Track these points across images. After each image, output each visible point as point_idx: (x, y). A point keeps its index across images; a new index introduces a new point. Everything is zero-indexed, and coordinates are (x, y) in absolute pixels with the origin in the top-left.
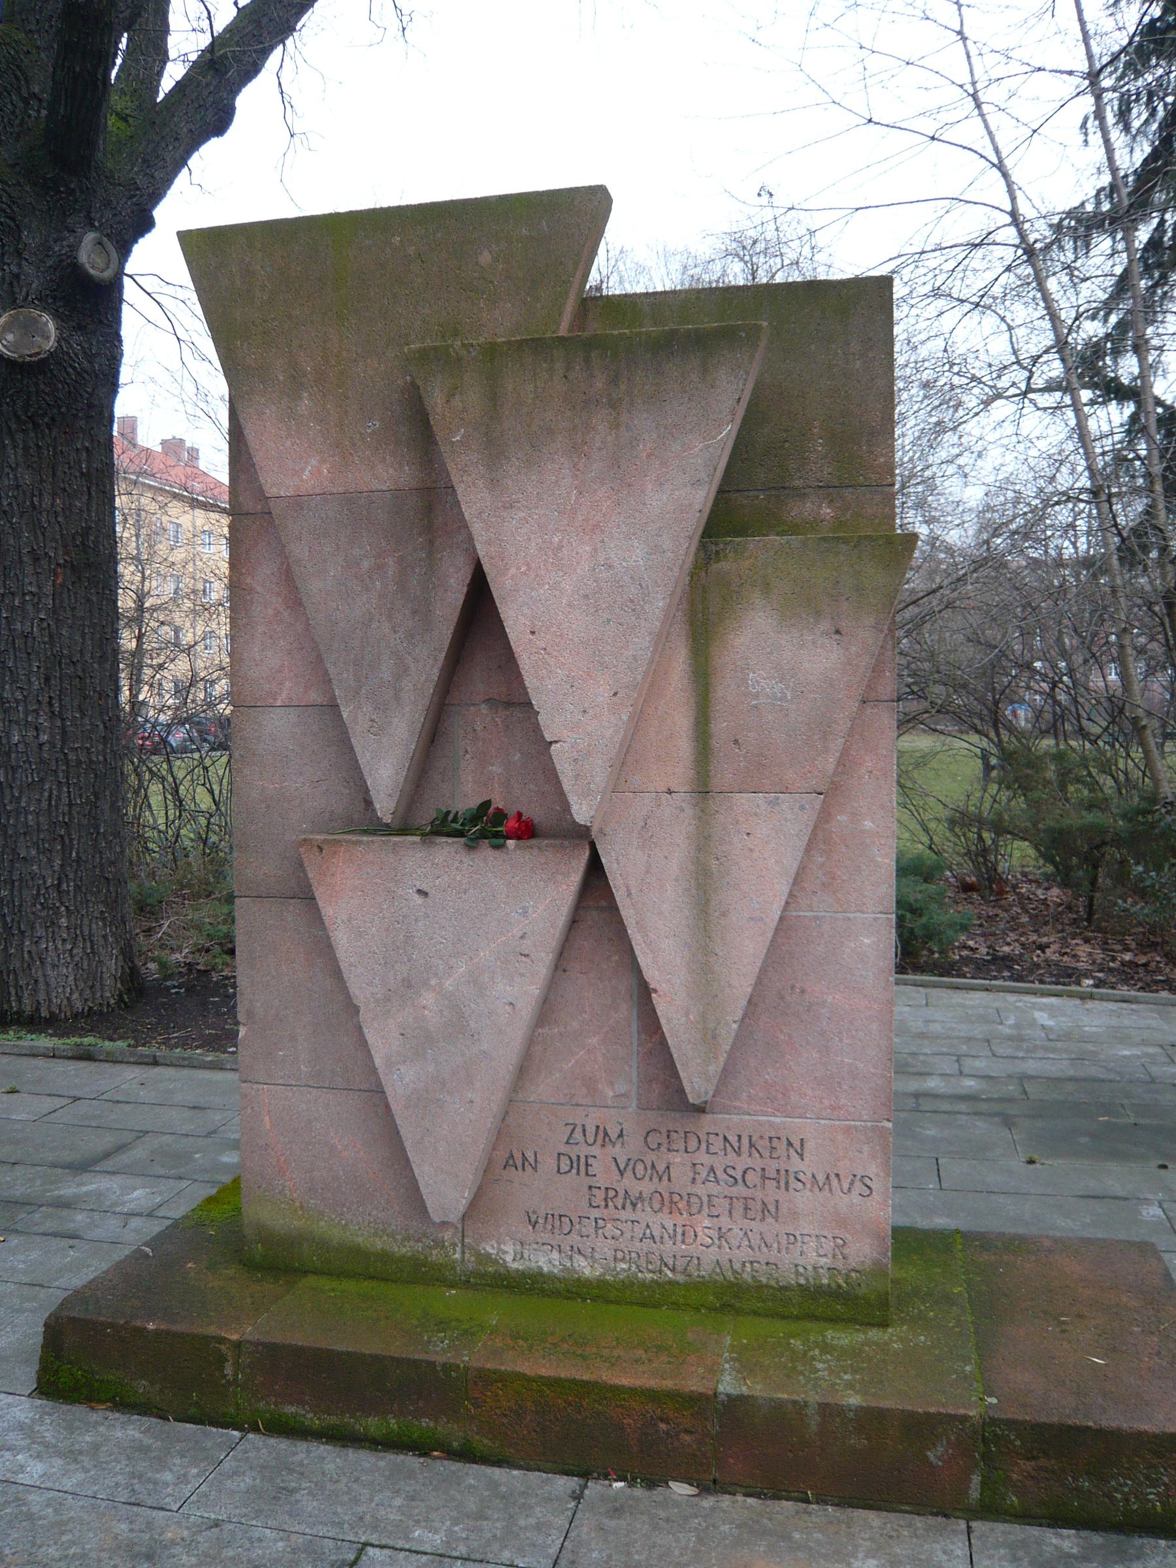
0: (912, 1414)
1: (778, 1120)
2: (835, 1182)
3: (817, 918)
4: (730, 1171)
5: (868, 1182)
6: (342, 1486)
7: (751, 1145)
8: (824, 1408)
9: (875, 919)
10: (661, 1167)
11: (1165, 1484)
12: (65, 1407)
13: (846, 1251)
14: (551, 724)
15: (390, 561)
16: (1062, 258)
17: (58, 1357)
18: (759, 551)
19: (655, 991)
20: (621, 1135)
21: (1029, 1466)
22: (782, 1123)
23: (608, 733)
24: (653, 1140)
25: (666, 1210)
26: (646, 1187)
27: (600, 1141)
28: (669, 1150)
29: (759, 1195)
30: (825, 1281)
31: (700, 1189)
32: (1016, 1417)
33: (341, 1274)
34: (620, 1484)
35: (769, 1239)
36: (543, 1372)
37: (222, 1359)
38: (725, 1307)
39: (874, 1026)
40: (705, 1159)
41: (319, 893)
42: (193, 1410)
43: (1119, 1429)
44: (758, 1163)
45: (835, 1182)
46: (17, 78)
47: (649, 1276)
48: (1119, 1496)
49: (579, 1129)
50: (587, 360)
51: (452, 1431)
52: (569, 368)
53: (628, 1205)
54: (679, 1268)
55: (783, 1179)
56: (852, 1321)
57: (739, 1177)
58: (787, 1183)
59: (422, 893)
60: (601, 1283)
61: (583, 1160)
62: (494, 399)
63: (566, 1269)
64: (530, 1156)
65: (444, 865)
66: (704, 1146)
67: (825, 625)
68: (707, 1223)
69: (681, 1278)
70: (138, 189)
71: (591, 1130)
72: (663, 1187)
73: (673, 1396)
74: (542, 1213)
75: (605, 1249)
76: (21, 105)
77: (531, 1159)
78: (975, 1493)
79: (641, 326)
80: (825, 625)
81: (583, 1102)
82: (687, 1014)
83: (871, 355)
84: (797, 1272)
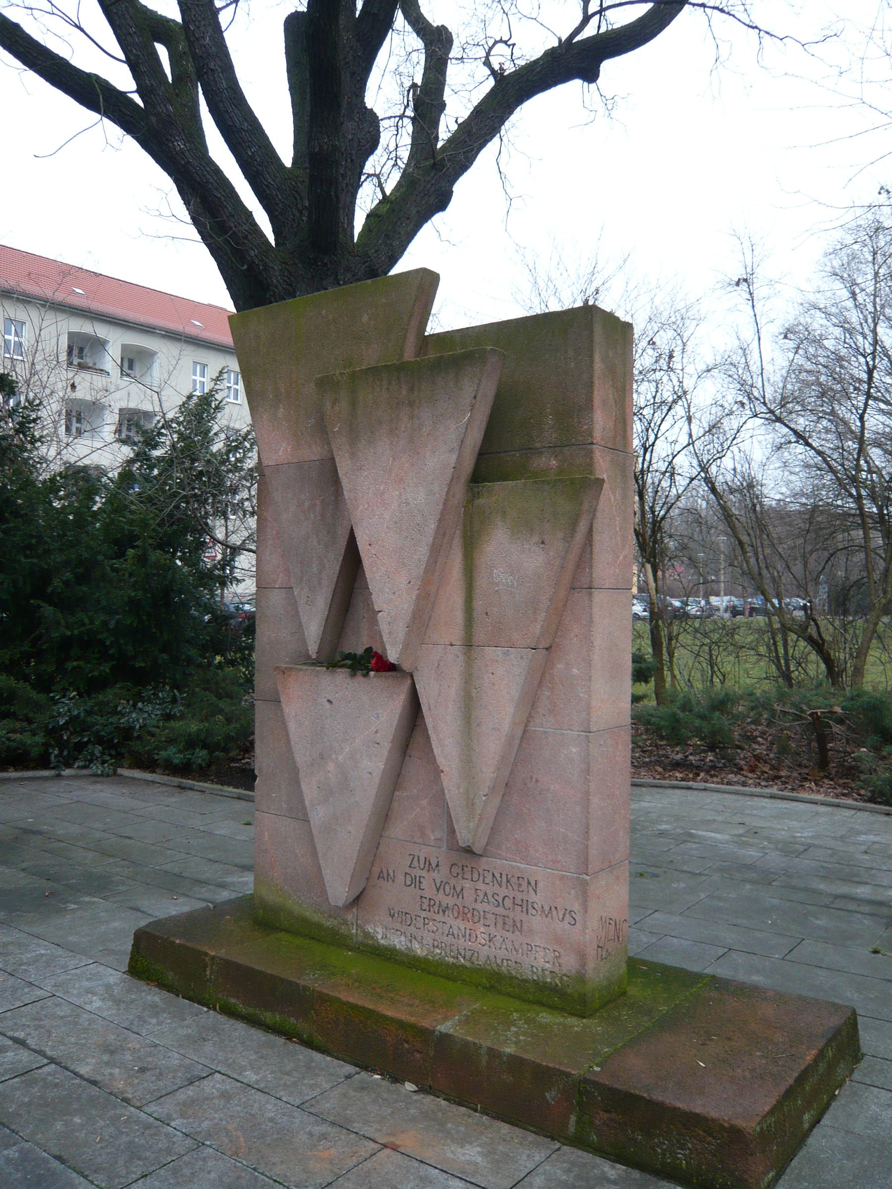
0: (539, 1066)
1: (523, 866)
2: (554, 913)
3: (545, 732)
5: (574, 916)
6: (232, 1044)
7: (508, 881)
8: (490, 1050)
9: (579, 736)
10: (458, 889)
11: (689, 1149)
12: (135, 981)
13: (561, 961)
15: (318, 502)
17: (138, 953)
18: (498, 492)
19: (442, 771)
20: (437, 866)
21: (606, 1116)
22: (525, 868)
23: (406, 606)
24: (455, 870)
25: (460, 918)
26: (450, 901)
27: (426, 868)
29: (511, 915)
30: (549, 980)
31: (479, 907)
32: (601, 1081)
33: (296, 933)
34: (379, 1077)
35: (517, 945)
36: (351, 1000)
37: (206, 966)
38: (491, 988)
39: (578, 809)
42: (191, 993)
43: (662, 1103)
45: (554, 913)
46: (295, 198)
47: (451, 960)
48: (659, 1151)
49: (416, 859)
50: (398, 378)
51: (303, 1026)
52: (390, 383)
53: (441, 911)
54: (467, 958)
55: (525, 906)
56: (563, 1010)
57: (500, 901)
58: (527, 910)
60: (425, 960)
62: (354, 404)
63: (408, 948)
64: (391, 872)
65: (339, 685)
66: (481, 878)
67: (536, 538)
68: (482, 930)
69: (468, 964)
70: (369, 257)
73: (413, 1027)
74: (396, 910)
75: (428, 939)
76: (298, 214)
77: (392, 875)
78: (572, 1128)
79: (426, 355)
80: (536, 538)
81: (418, 841)
82: (458, 788)
83: (580, 358)
84: (532, 971)
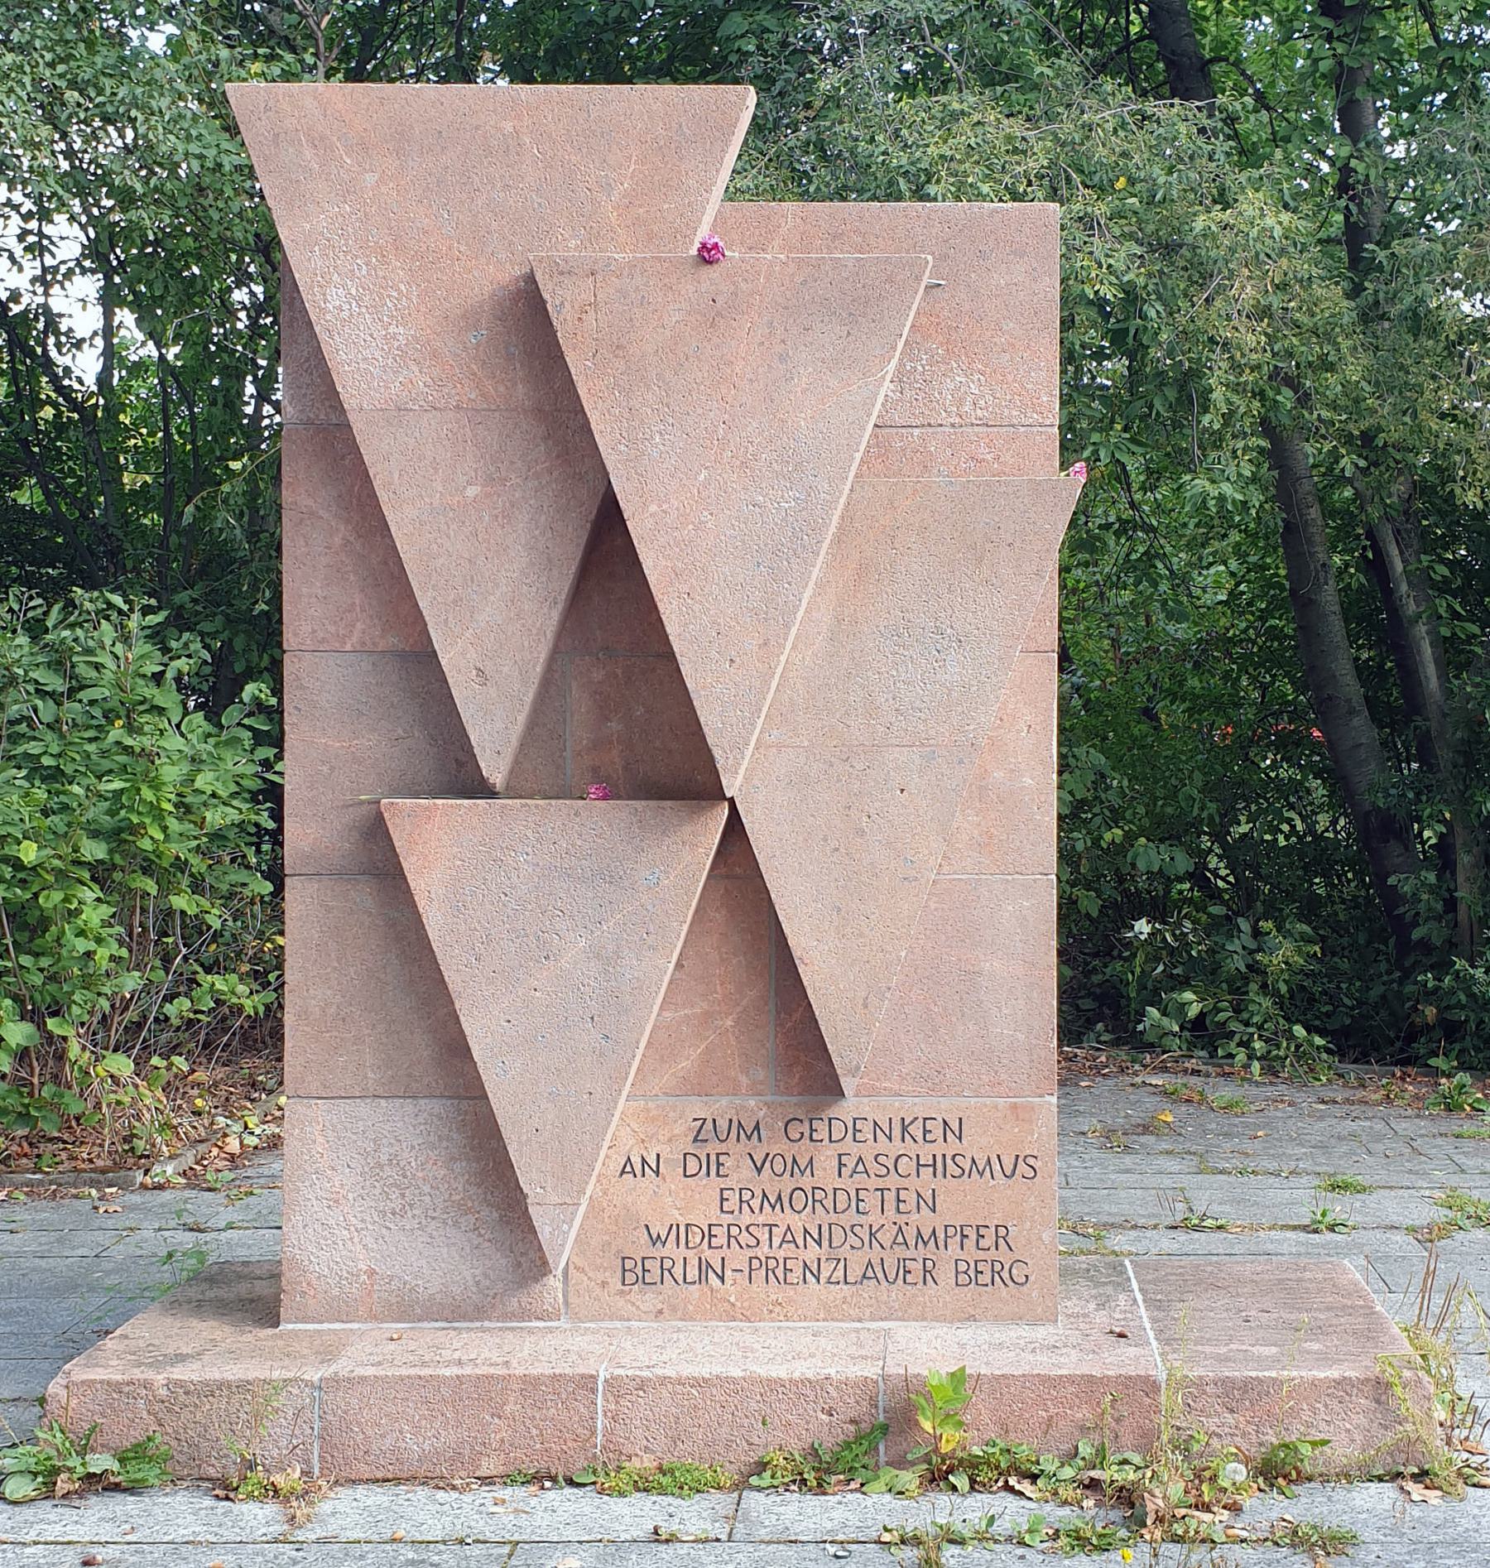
4: (881, 1159)
20: (757, 1127)
28: (811, 1140)
40: (855, 1149)
44: (911, 1148)
57: (891, 1167)
61: (713, 1158)
71: (723, 1124)
72: (806, 1182)
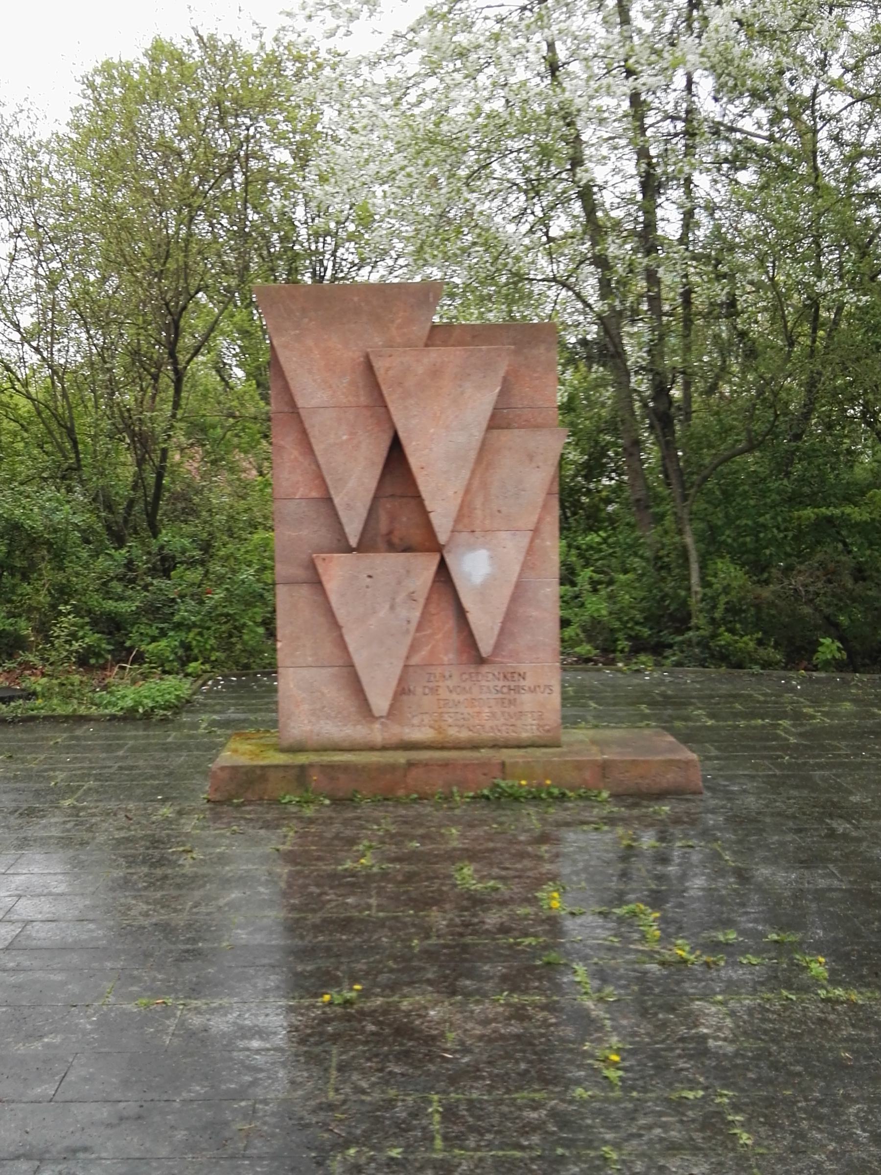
14: (429, 505)
16: (828, 372)
26: (461, 698)
31: (484, 696)
41: (324, 579)
44: (507, 683)
59: (370, 577)
